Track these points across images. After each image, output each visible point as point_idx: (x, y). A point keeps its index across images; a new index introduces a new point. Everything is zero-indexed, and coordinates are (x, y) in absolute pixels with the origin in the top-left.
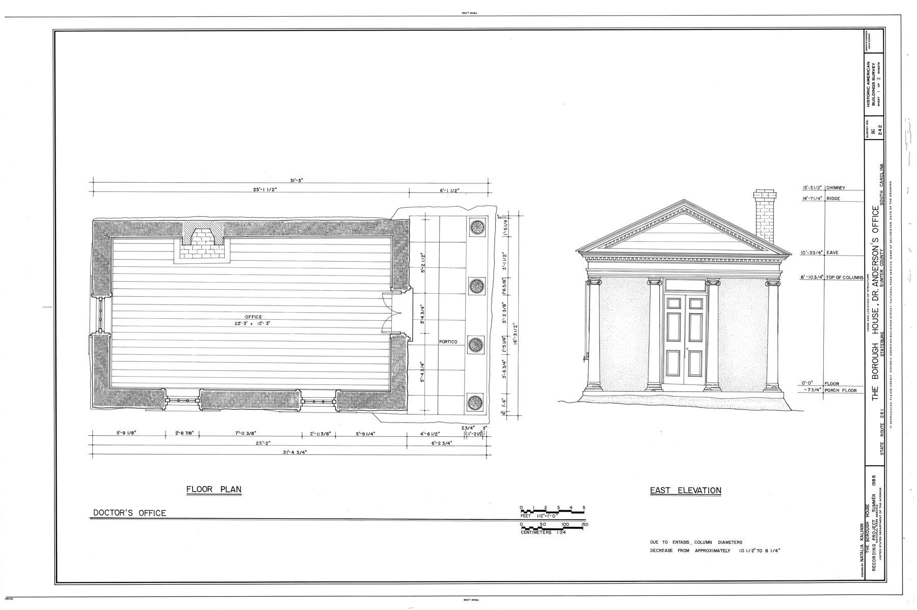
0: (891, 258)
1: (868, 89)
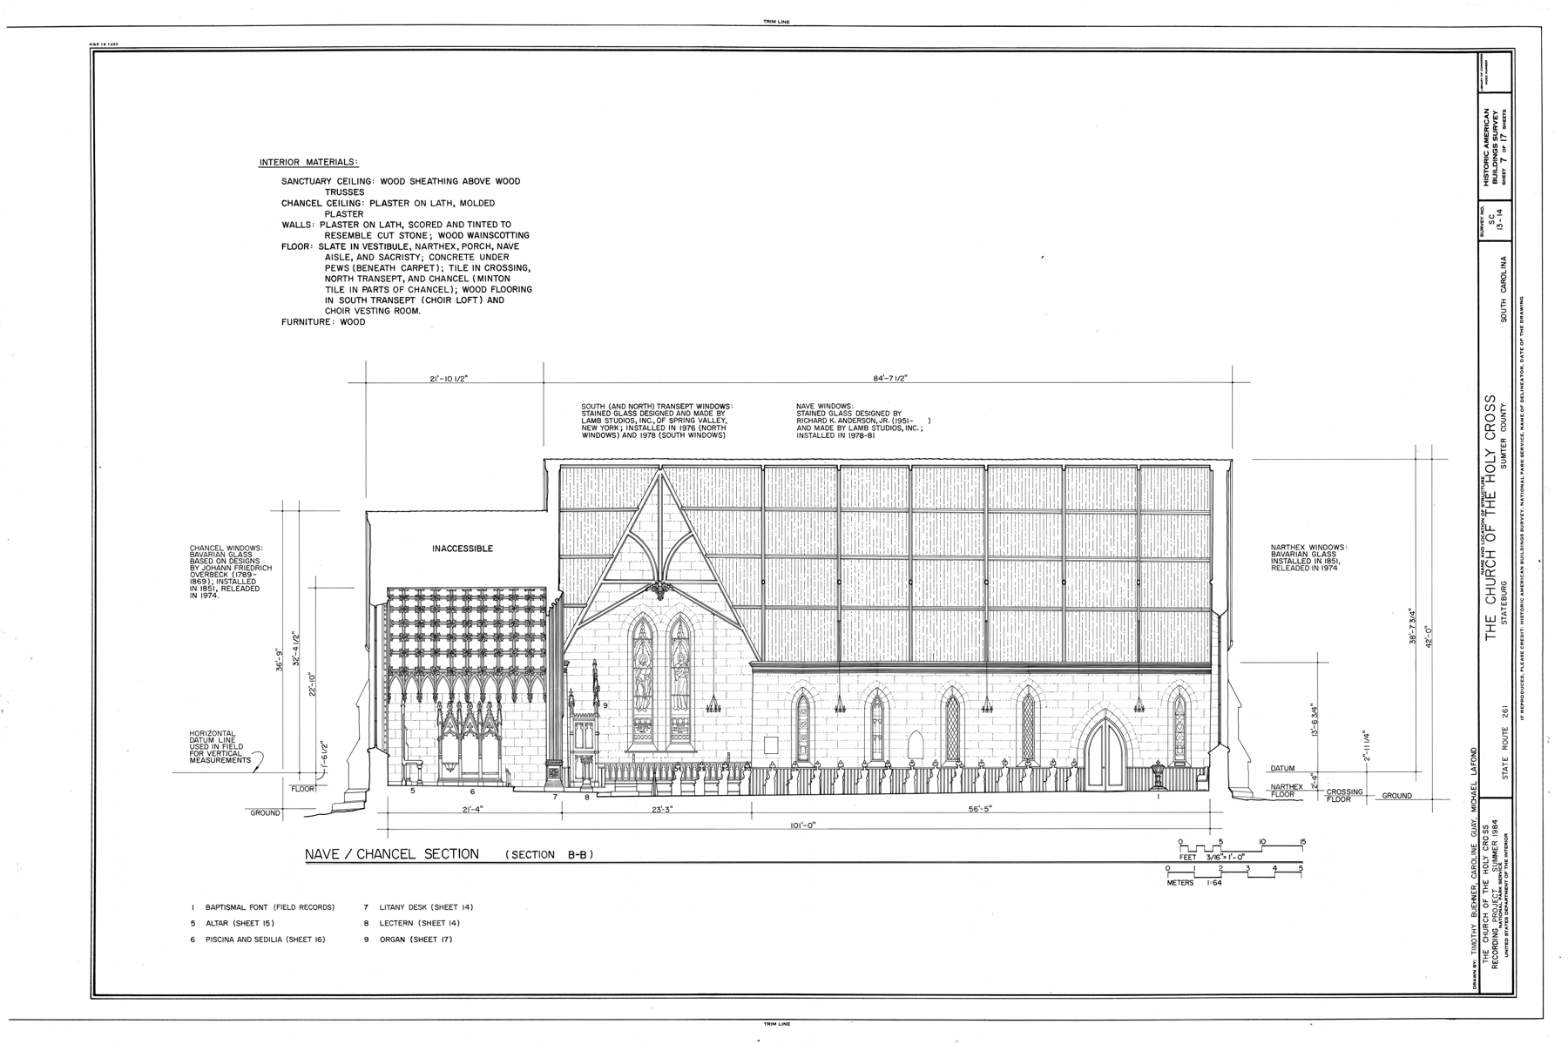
1: (1486, 156)
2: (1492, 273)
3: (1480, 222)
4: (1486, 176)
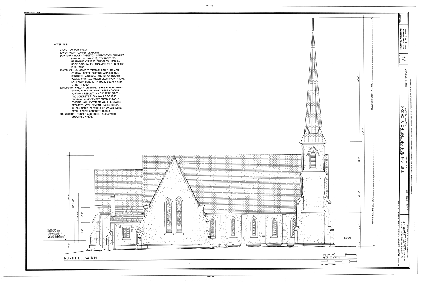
0: (411, 115)
1: (401, 41)
3: (399, 59)
4: (401, 47)
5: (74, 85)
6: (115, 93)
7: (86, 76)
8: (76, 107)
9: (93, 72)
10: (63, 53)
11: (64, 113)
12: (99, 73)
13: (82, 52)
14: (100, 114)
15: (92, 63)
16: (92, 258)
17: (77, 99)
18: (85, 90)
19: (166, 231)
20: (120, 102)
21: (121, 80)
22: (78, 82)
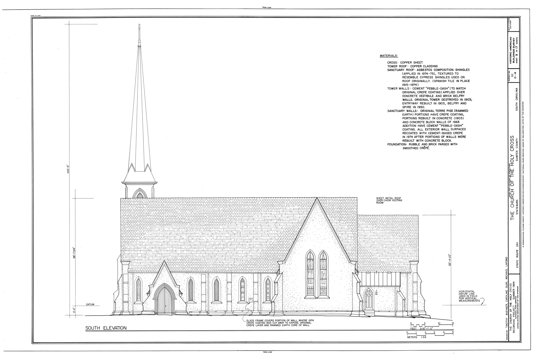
0: (523, 147)
1: (511, 53)
2: (512, 94)
3: (508, 76)
4: (511, 60)
5: (405, 107)
6: (458, 118)
7: (421, 95)
8: (408, 135)
9: (430, 90)
10: (392, 67)
11: (392, 143)
12: (437, 92)
13: (417, 66)
14: (437, 144)
15: (429, 79)
16: (120, 328)
17: (410, 126)
18: (419, 114)
19: (320, 293)
20: (464, 129)
21: (467, 101)
22: (410, 104)
